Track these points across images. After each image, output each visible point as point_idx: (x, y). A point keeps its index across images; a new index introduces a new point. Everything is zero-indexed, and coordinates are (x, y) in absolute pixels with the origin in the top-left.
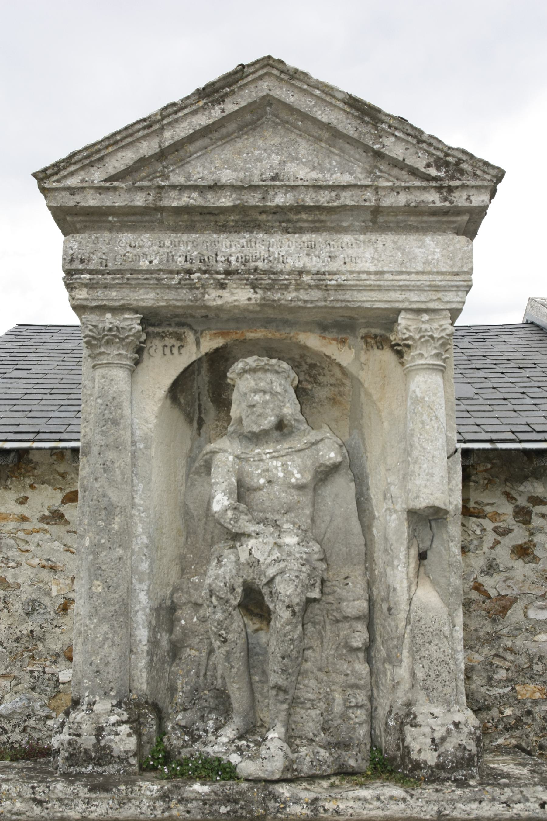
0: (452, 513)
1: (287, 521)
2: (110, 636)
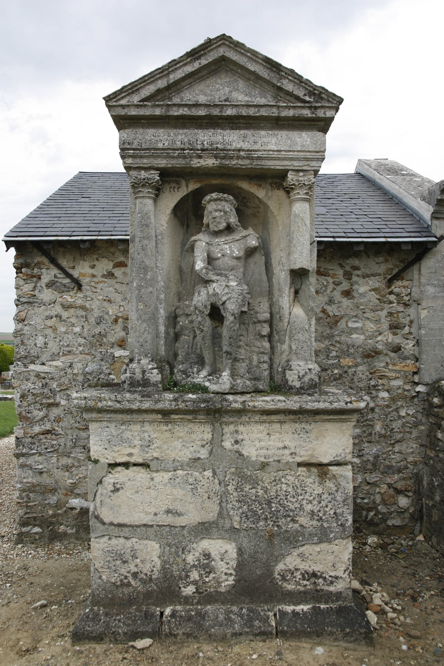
0: (311, 271)
1: (232, 275)
2: (147, 329)
